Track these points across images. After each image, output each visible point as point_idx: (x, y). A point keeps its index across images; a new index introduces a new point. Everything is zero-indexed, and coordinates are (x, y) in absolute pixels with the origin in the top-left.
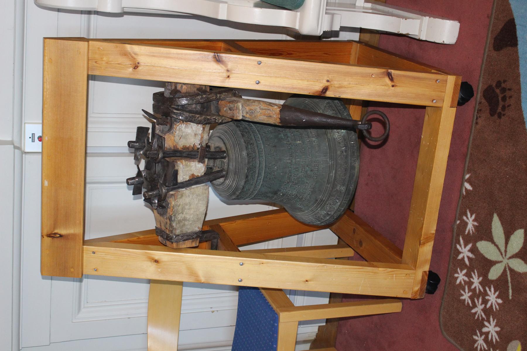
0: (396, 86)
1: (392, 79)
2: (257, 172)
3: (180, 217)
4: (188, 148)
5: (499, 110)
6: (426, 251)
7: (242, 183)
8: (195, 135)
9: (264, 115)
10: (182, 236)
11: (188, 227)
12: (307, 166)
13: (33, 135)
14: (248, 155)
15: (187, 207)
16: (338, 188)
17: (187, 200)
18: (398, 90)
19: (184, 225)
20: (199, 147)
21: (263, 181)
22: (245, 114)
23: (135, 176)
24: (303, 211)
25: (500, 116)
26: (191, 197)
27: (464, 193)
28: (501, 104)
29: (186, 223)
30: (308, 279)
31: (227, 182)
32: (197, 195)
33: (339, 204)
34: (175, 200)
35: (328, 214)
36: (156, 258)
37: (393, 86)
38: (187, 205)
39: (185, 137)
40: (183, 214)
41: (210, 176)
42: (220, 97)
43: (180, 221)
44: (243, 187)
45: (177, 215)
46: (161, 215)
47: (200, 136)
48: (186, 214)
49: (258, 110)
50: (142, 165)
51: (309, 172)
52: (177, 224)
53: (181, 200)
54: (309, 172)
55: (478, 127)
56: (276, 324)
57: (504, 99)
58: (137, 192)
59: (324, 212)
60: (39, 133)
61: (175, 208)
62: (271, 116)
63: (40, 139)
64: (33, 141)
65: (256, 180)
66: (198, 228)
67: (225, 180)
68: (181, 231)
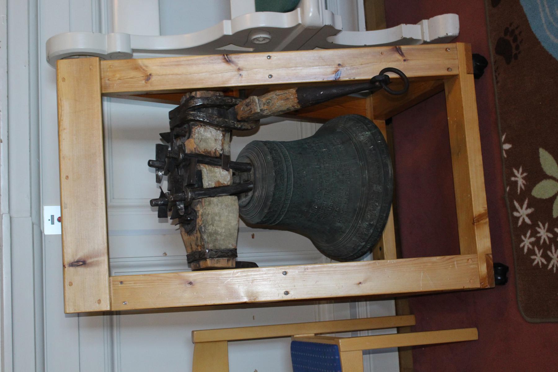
0: (408, 60)
1: (402, 54)
2: (286, 176)
3: (211, 229)
4: (210, 152)
5: (514, 52)
6: (483, 241)
7: (272, 189)
8: (216, 140)
9: (282, 99)
10: (216, 252)
11: (222, 242)
12: (338, 171)
13: (52, 217)
14: (273, 158)
15: (217, 218)
16: (374, 188)
17: (216, 210)
18: (411, 63)
19: (216, 240)
20: (221, 152)
21: (294, 187)
22: (262, 107)
23: (158, 198)
24: (344, 232)
25: (516, 57)
26: (220, 207)
27: (505, 156)
28: (514, 45)
29: (219, 237)
30: (361, 281)
31: (256, 194)
32: (226, 206)
33: (379, 208)
34: (203, 207)
35: (370, 225)
36: (191, 280)
37: (405, 60)
38: (216, 215)
39: (206, 140)
40: (213, 226)
41: (236, 190)
42: (235, 101)
43: (211, 235)
44: (274, 195)
45: (207, 226)
46: (189, 232)
47: (220, 142)
48: (217, 226)
49: (275, 97)
50: (165, 185)
51: (340, 177)
52: (208, 237)
53: (209, 208)
54: (340, 177)
55: (499, 84)
56: (337, 357)
57: (515, 40)
58: (162, 215)
59: (365, 224)
60: (57, 215)
61: (204, 217)
62: (288, 99)
63: (60, 220)
64: (53, 223)
65: (285, 184)
66: (232, 245)
67: (254, 192)
68: (214, 246)
